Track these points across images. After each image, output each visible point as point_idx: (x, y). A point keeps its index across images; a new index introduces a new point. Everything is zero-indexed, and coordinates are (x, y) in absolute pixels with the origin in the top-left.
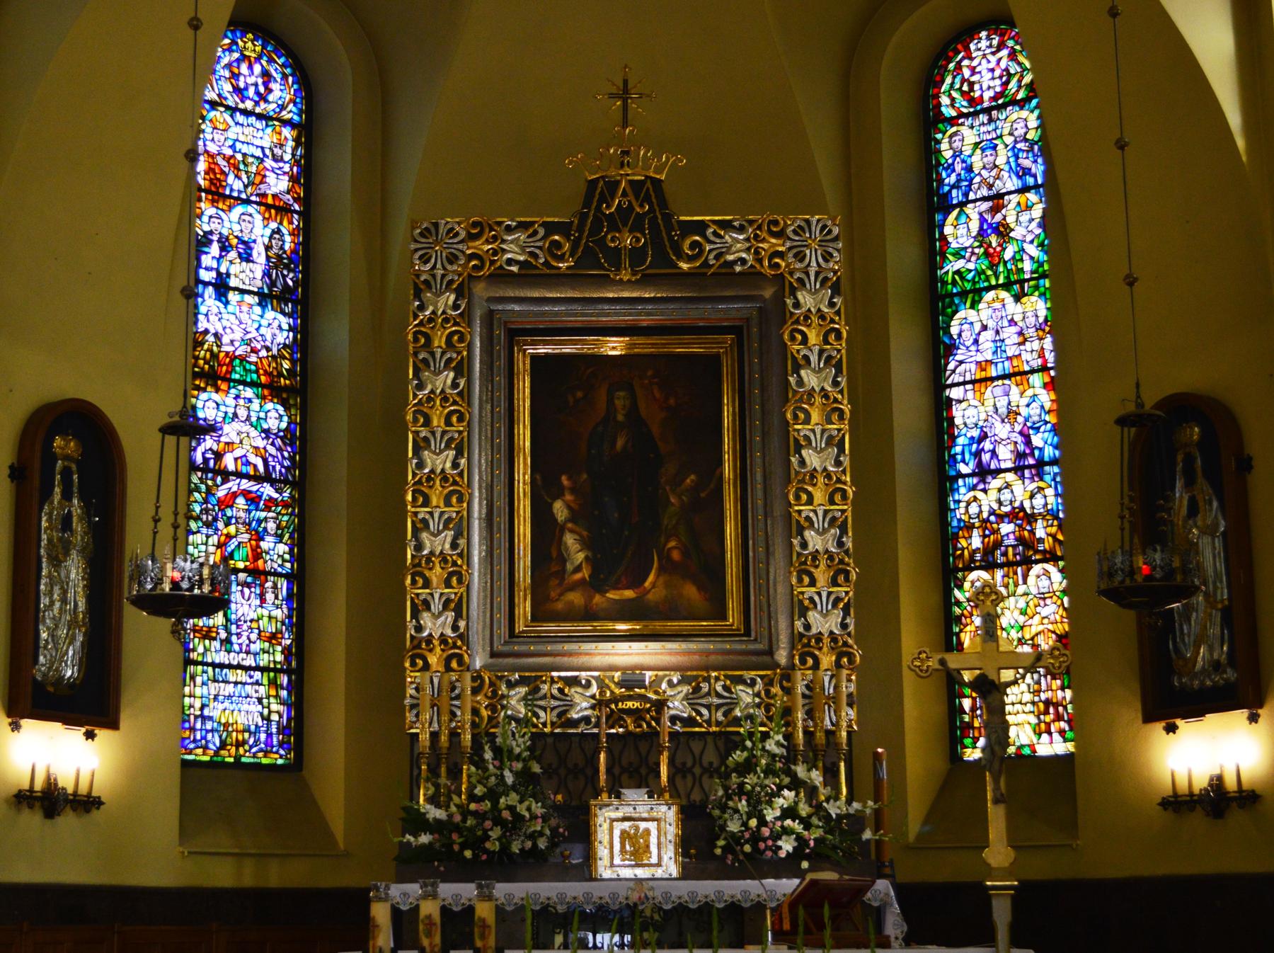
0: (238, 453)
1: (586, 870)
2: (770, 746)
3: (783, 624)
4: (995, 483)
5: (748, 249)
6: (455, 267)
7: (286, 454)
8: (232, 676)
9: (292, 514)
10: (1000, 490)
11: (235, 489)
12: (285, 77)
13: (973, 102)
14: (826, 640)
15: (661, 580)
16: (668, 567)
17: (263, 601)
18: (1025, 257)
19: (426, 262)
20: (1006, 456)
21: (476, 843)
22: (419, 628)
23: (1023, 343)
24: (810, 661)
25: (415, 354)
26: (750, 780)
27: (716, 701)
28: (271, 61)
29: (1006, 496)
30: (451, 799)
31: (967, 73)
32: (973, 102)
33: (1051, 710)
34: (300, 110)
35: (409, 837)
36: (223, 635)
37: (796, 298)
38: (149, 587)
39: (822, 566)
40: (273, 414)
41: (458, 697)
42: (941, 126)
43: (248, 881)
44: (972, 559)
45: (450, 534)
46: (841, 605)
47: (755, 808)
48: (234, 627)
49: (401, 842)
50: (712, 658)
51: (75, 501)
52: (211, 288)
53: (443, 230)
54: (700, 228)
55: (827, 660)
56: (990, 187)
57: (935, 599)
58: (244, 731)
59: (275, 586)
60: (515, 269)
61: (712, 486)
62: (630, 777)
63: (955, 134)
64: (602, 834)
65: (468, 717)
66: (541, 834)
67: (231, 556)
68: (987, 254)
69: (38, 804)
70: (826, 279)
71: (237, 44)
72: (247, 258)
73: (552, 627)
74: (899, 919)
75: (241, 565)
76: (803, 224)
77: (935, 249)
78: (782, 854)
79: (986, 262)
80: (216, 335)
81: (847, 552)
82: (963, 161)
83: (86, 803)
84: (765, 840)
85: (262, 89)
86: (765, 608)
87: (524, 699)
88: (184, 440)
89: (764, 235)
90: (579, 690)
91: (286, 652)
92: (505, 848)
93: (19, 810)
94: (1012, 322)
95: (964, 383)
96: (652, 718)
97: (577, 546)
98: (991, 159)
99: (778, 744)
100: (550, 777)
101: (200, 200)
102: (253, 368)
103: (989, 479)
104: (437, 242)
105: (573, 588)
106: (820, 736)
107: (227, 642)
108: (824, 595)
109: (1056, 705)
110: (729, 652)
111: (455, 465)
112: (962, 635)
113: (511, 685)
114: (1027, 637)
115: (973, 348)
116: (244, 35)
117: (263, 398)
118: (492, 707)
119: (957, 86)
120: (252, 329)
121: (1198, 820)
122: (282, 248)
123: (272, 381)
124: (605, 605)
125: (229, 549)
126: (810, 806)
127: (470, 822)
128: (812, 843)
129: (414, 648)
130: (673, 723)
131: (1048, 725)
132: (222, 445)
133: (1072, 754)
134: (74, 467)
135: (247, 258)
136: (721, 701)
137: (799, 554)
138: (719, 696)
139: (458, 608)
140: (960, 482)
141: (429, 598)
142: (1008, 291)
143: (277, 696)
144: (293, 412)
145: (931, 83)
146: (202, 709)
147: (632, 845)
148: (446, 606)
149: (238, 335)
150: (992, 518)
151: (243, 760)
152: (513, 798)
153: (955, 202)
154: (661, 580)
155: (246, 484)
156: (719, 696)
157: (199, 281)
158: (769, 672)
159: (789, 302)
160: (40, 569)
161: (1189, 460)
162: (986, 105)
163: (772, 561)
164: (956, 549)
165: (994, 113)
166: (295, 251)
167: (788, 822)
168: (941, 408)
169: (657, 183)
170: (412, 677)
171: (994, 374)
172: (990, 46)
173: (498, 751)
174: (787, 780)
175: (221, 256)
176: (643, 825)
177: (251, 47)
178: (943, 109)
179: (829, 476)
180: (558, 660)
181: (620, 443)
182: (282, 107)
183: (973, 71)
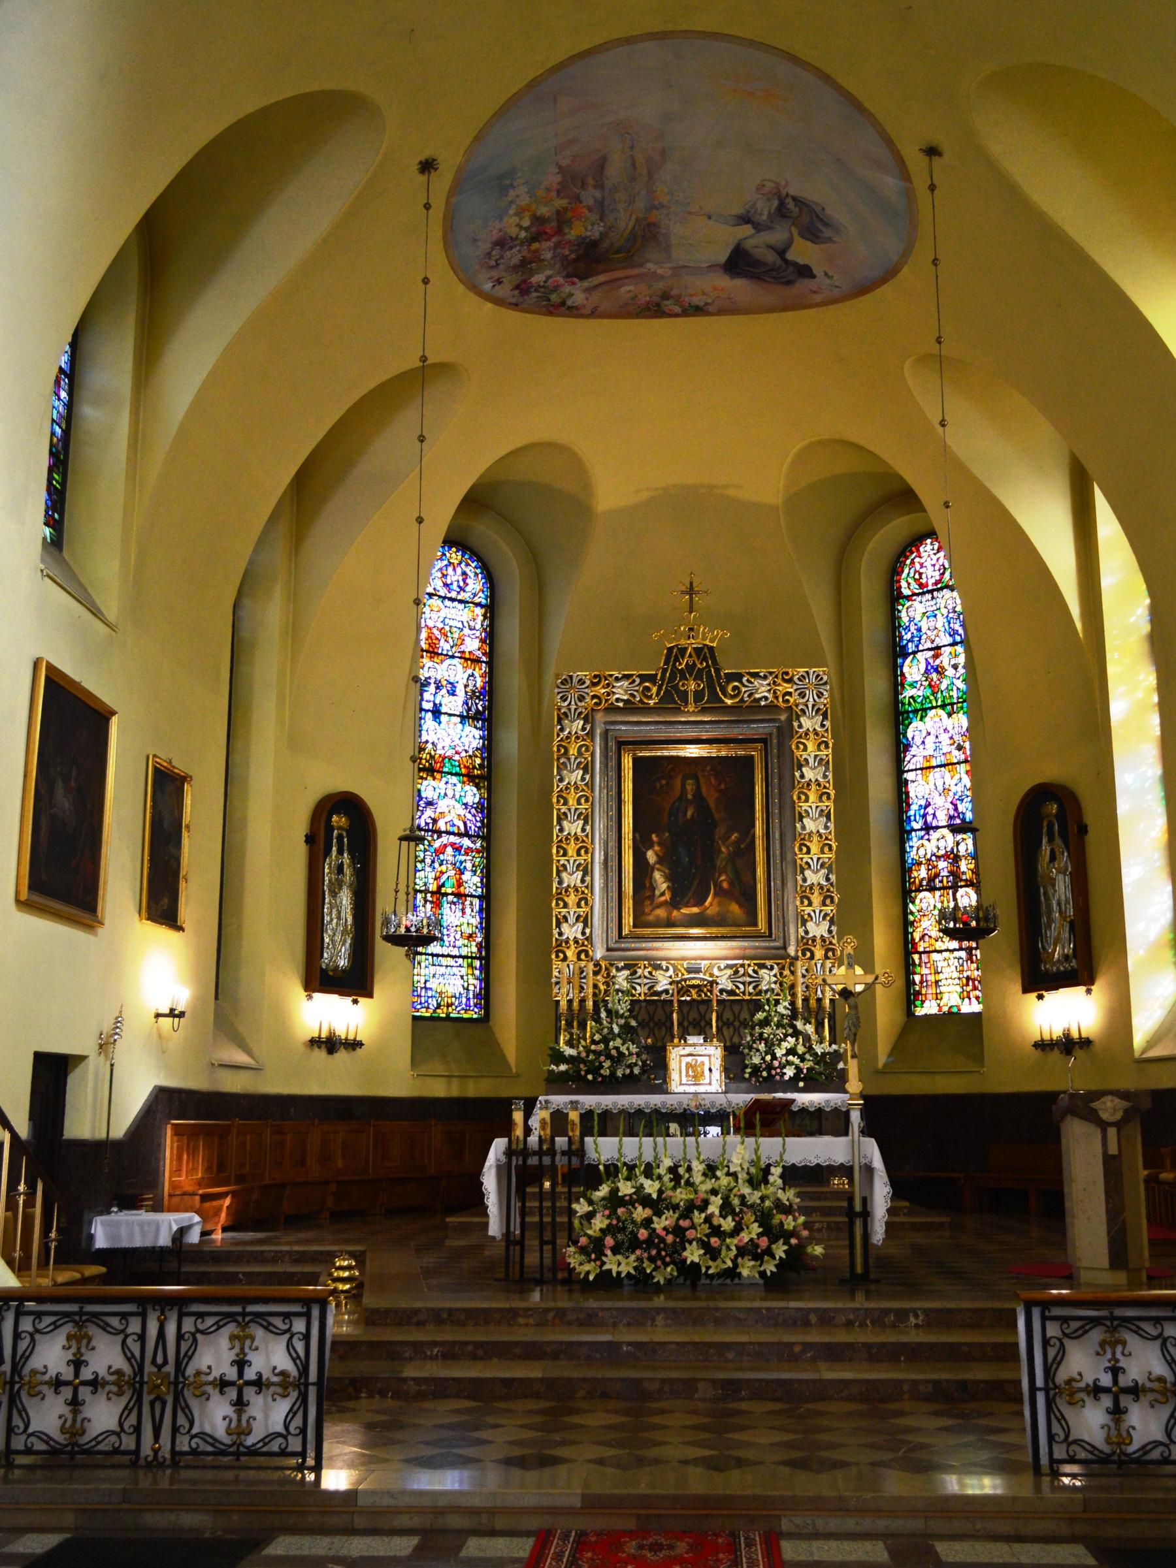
0: (447, 819)
1: (663, 1089)
2: (780, 1009)
3: (792, 930)
4: (934, 835)
5: (769, 691)
6: (583, 704)
7: (478, 819)
8: (444, 961)
9: (482, 857)
10: (938, 840)
11: (445, 842)
12: (476, 575)
13: (921, 586)
14: (818, 941)
15: (716, 901)
16: (720, 892)
17: (464, 913)
18: (955, 688)
19: (565, 701)
20: (942, 820)
21: (596, 1070)
22: (561, 934)
24: (808, 954)
25: (558, 759)
26: (767, 1031)
27: (748, 979)
28: (467, 565)
29: (942, 844)
31: (917, 566)
33: (971, 983)
34: (487, 596)
35: (553, 1067)
37: (799, 721)
38: (393, 930)
39: (816, 894)
40: (469, 793)
41: (585, 978)
42: (901, 601)
43: (455, 1092)
44: (921, 885)
45: (580, 874)
46: (828, 918)
47: (770, 1048)
49: (548, 1070)
51: (345, 855)
52: (430, 713)
53: (575, 680)
55: (819, 953)
56: (933, 642)
57: (897, 911)
59: (471, 904)
60: (621, 704)
61: (748, 840)
62: (694, 1028)
63: (911, 606)
64: (673, 1064)
65: (591, 990)
66: (636, 1064)
67: (443, 885)
69: (323, 1046)
70: (819, 710)
71: (445, 555)
72: (452, 693)
73: (648, 931)
75: (449, 891)
76: (804, 674)
77: (897, 682)
78: (786, 1078)
80: (433, 743)
81: (832, 884)
83: (354, 1045)
84: (775, 1069)
85: (461, 584)
88: (412, 844)
89: (779, 681)
90: (662, 972)
91: (479, 946)
92: (613, 1074)
93: (312, 1050)
94: (945, 730)
95: (916, 770)
96: (708, 990)
97: (662, 880)
98: (933, 623)
99: (785, 1008)
101: (422, 657)
102: (457, 764)
103: (931, 832)
104: (571, 688)
105: (659, 906)
106: (813, 1003)
108: (817, 912)
109: (974, 980)
110: (757, 948)
111: (583, 830)
112: (915, 934)
113: (618, 970)
115: (922, 747)
116: (450, 549)
117: (464, 783)
118: (607, 984)
119: (911, 575)
120: (456, 739)
121: (1056, 1055)
122: (475, 686)
125: (442, 881)
126: (805, 1047)
127: (591, 1057)
128: (805, 1071)
129: (558, 946)
130: (721, 994)
131: (968, 993)
132: (437, 814)
134: (345, 834)
135: (452, 693)
137: (801, 886)
138: (750, 976)
139: (586, 921)
140: (913, 833)
141: (567, 915)
143: (473, 974)
144: (482, 791)
145: (895, 571)
146: (425, 983)
147: (694, 1071)
148: (577, 919)
149: (447, 743)
150: (933, 858)
151: (452, 1015)
152: (618, 1042)
153: (910, 651)
154: (716, 901)
155: (453, 839)
156: (750, 976)
157: (421, 710)
159: (796, 724)
160: (324, 899)
161: (1051, 825)
162: (930, 588)
163: (786, 890)
164: (910, 877)
165: (935, 593)
166: (483, 688)
167: (790, 1058)
168: (901, 785)
169: (711, 649)
170: (557, 965)
171: (934, 764)
172: (933, 549)
173: (609, 1012)
174: (790, 1031)
175: (436, 693)
176: (700, 1059)
177: (455, 556)
178: (903, 590)
179: (820, 836)
181: (689, 813)
182: (475, 595)
183: (922, 565)
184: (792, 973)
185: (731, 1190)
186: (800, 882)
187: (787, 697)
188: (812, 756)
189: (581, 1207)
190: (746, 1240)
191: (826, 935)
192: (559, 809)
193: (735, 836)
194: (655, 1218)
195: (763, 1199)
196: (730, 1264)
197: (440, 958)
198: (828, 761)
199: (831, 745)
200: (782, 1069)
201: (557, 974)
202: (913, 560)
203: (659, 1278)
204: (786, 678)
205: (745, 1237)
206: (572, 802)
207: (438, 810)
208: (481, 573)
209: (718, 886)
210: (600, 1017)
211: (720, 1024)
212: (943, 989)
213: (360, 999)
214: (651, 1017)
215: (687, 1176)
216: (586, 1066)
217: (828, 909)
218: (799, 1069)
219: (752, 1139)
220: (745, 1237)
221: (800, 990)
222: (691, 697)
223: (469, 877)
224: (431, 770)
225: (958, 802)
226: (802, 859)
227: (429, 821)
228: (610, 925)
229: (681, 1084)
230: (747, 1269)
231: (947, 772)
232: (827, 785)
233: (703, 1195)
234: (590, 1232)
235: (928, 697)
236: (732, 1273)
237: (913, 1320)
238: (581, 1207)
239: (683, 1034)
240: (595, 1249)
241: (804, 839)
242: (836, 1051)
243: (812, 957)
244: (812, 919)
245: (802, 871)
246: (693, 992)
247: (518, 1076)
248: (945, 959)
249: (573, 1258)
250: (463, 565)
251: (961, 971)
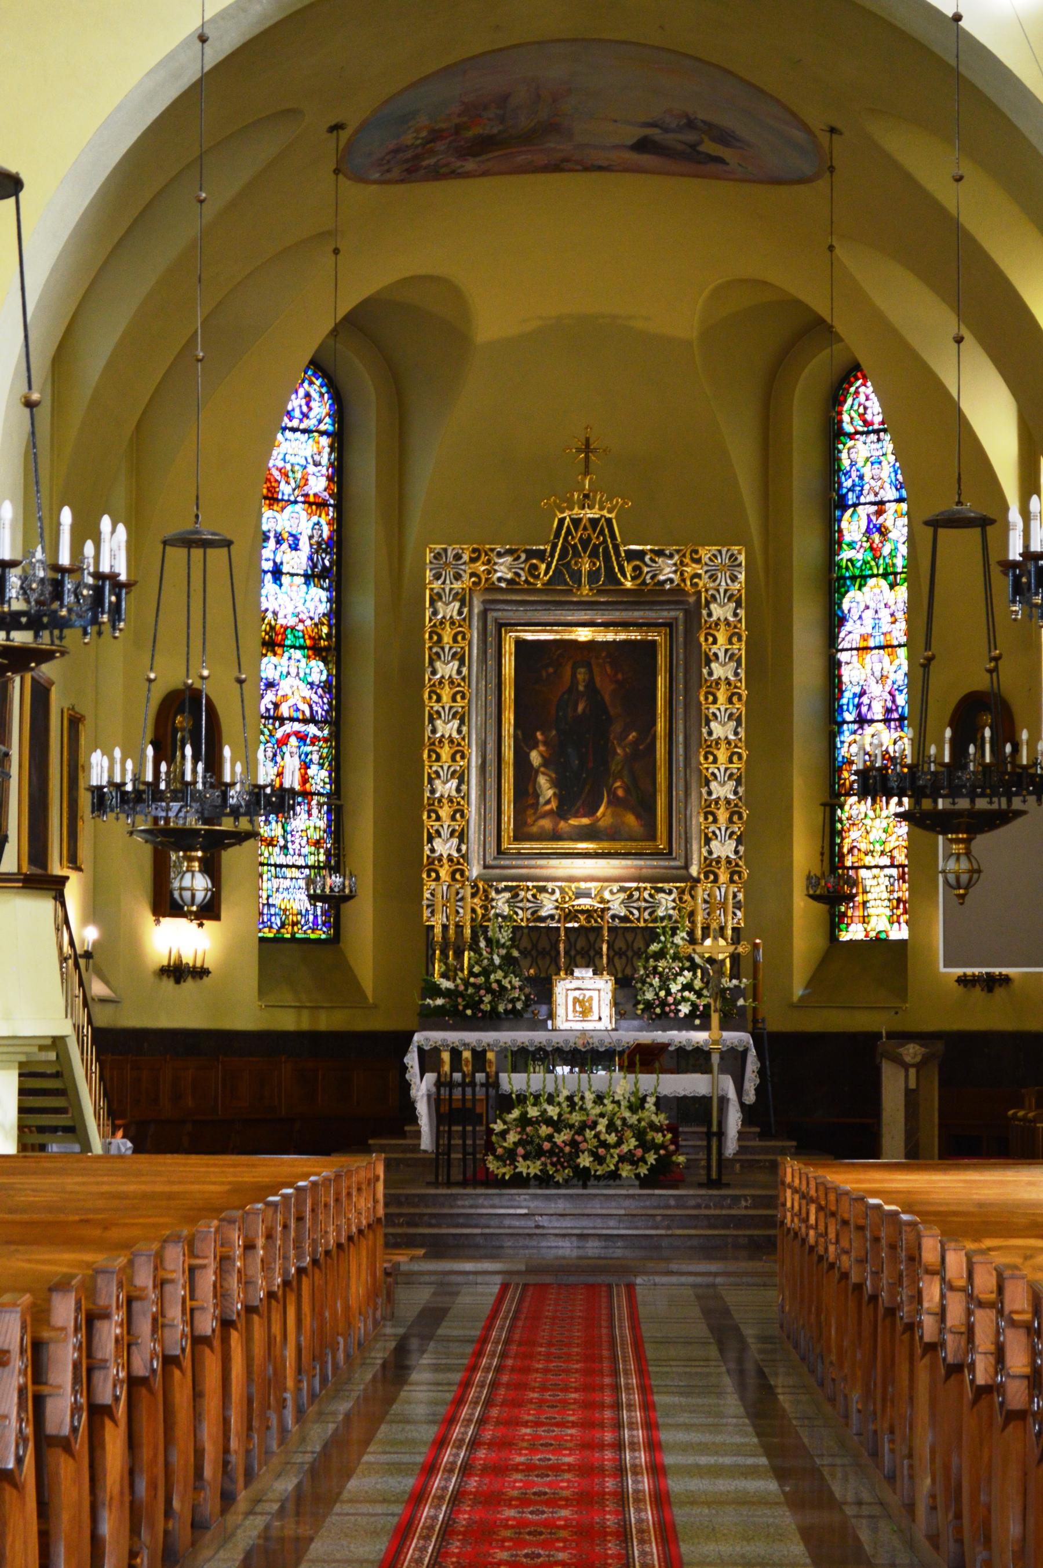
0: (291, 702)
3: (695, 847)
4: (869, 730)
5: (675, 572)
7: (325, 700)
9: (330, 747)
10: (873, 736)
11: (289, 731)
12: (322, 395)
13: (866, 423)
14: (723, 862)
16: (615, 802)
17: (310, 815)
20: (878, 712)
21: (475, 1005)
22: (433, 850)
23: (893, 623)
24: (712, 877)
26: (662, 964)
27: (644, 904)
30: (457, 974)
32: (866, 423)
33: (901, 906)
35: (428, 1001)
36: (282, 842)
40: (316, 670)
42: (842, 438)
43: (305, 1025)
47: (665, 983)
48: (289, 837)
49: (423, 1005)
50: (644, 871)
54: (640, 555)
56: (876, 494)
58: (297, 914)
60: (503, 585)
61: (648, 741)
62: (583, 957)
63: (853, 447)
65: (468, 917)
66: (518, 999)
68: (872, 548)
72: (295, 547)
74: (756, 1059)
76: (716, 553)
77: (833, 541)
78: (681, 1015)
79: (871, 555)
82: (858, 470)
83: (200, 973)
84: (669, 1005)
85: (305, 409)
86: (683, 836)
87: (507, 901)
89: (687, 560)
90: (547, 895)
91: (328, 853)
92: (494, 1009)
93: (161, 979)
95: (851, 649)
96: (599, 916)
97: (548, 785)
99: (683, 939)
100: (525, 957)
102: (301, 634)
103: (866, 726)
105: (544, 816)
107: (285, 847)
109: (905, 902)
110: (655, 867)
113: (498, 891)
114: (887, 850)
115: (859, 622)
117: (309, 657)
118: (485, 908)
120: (300, 604)
122: (321, 536)
123: (315, 644)
124: (567, 829)
127: (470, 991)
128: (701, 1008)
129: (430, 864)
130: (613, 920)
132: (279, 697)
133: (906, 940)
135: (295, 547)
136: (647, 905)
138: (646, 901)
139: (462, 837)
140: (845, 727)
142: (886, 579)
144: (330, 666)
146: (268, 899)
147: (581, 1006)
148: (452, 834)
149: (290, 610)
151: (297, 936)
153: (850, 503)
154: (609, 811)
155: (297, 726)
156: (646, 901)
158: (682, 885)
162: (876, 426)
164: (840, 779)
166: (330, 538)
167: (686, 994)
168: (833, 668)
170: (429, 885)
173: (489, 941)
174: (687, 964)
176: (588, 994)
179: (729, 743)
180: (532, 871)
181: (580, 708)
182: (320, 421)
184: (692, 897)
185: (615, 1114)
186: (705, 796)
187: (696, 580)
188: (723, 650)
189: (498, 1127)
190: (626, 1150)
192: (432, 707)
193: (633, 735)
194: (556, 1134)
195: (639, 1121)
196: (613, 1167)
197: (284, 869)
198: (740, 657)
199: (744, 638)
202: (857, 388)
203: (559, 1178)
205: (625, 1148)
206: (446, 698)
207: (280, 693)
208: (327, 392)
209: (612, 793)
211: (612, 954)
212: (871, 911)
213: (205, 922)
214: (535, 946)
215: (580, 1103)
216: (464, 1000)
218: (694, 1006)
219: (633, 1076)
220: (625, 1148)
221: (699, 918)
222: (584, 579)
223: (316, 772)
224: (273, 644)
225: (897, 693)
227: (271, 706)
229: (567, 1020)
230: (626, 1171)
231: (886, 656)
232: (739, 684)
233: (593, 1118)
234: (505, 1144)
235: (869, 563)
236: (614, 1175)
237: (743, 1203)
238: (498, 1127)
239: (570, 965)
240: (510, 1156)
241: (710, 746)
242: (736, 986)
245: (707, 783)
246: (582, 917)
247: (375, 1006)
248: (874, 877)
249: (492, 1165)
250: (306, 385)
251: (892, 892)
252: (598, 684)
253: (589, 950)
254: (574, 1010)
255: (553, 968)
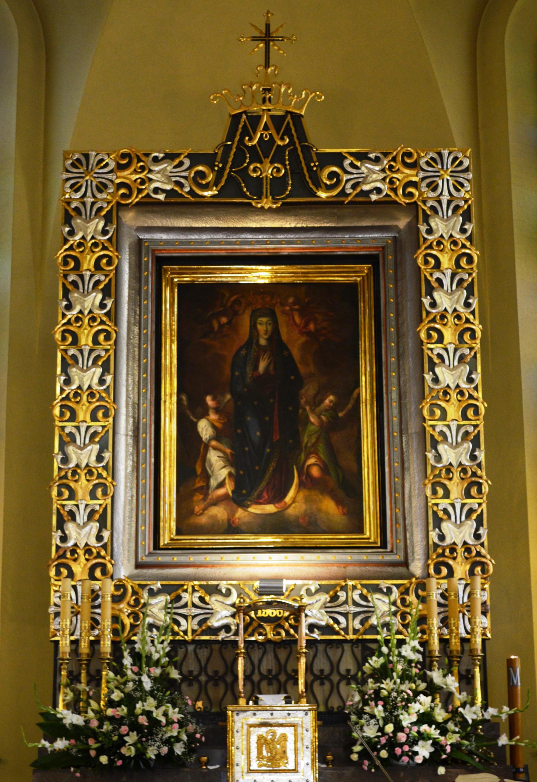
2: (406, 651)
6: (104, 196)
14: (460, 550)
15: (301, 495)
19: (77, 191)
26: (387, 685)
41: (99, 606)
46: (474, 516)
47: (391, 713)
60: (161, 197)
61: (350, 406)
66: (178, 739)
70: (457, 207)
73: (201, 539)
78: (419, 760)
84: (401, 745)
86: (401, 521)
90: (220, 598)
92: (141, 754)
97: (221, 463)
99: (414, 649)
105: (215, 503)
108: (458, 507)
113: (152, 594)
128: (448, 749)
129: (59, 557)
138: (355, 604)
147: (270, 751)
148: (91, 516)
152: (150, 704)
154: (301, 495)
156: (355, 604)
159: (423, 228)
163: (407, 476)
167: (425, 728)
173: (136, 657)
174: (423, 686)
176: (280, 731)
179: (461, 393)
181: (262, 366)
184: (423, 600)
187: (410, 189)
191: (471, 541)
200: (411, 746)
201: (57, 601)
204: (408, 161)
209: (305, 474)
210: (122, 665)
214: (203, 669)
216: (98, 742)
217: (472, 503)
222: (266, 188)
226: (433, 427)
228: (141, 528)
232: (471, 317)
243: (451, 573)
244: (449, 517)
245: (435, 444)
252: (284, 337)
253: (279, 674)
254: (260, 756)
255: (229, 696)
